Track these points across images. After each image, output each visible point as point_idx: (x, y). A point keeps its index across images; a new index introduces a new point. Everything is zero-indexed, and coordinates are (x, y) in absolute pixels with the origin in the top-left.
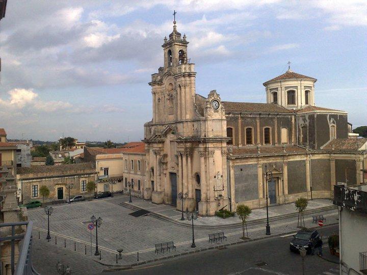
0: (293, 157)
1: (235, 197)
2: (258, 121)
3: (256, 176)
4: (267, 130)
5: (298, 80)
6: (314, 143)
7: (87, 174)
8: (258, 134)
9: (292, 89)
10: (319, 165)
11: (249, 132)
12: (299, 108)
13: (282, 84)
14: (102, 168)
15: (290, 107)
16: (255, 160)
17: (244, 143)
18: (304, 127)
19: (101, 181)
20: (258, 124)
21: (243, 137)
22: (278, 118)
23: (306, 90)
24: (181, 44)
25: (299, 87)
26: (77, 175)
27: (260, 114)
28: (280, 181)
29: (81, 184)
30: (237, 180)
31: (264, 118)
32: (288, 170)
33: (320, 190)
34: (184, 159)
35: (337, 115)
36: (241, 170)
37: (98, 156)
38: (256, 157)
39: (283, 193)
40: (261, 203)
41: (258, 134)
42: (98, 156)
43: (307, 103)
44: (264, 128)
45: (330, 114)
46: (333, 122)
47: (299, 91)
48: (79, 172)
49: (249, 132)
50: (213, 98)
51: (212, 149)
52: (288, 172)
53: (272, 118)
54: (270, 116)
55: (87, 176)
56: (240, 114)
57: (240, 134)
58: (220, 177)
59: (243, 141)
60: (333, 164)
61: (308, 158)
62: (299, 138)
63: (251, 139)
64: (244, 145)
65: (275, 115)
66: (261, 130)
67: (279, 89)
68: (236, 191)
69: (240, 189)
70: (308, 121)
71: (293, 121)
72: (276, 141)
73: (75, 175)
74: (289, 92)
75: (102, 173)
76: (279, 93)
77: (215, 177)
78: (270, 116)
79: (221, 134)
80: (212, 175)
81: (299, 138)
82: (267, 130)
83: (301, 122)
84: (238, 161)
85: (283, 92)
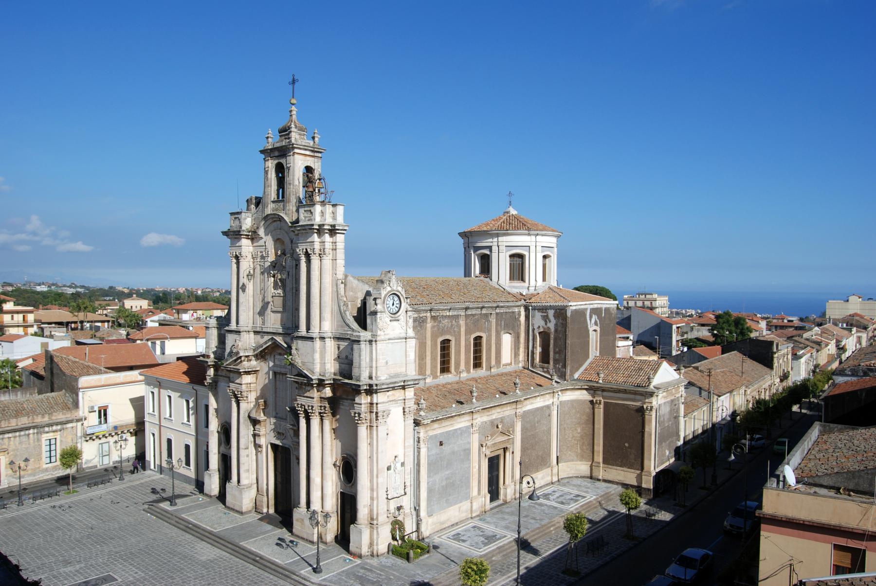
0: (531, 401)
1: (427, 504)
2: (462, 322)
3: (467, 452)
4: (478, 341)
5: (529, 235)
6: (564, 366)
7: (57, 424)
8: (461, 353)
10: (574, 411)
11: (445, 345)
12: (532, 289)
13: (500, 239)
14: (93, 407)
15: (514, 287)
16: (467, 418)
17: (436, 373)
19: (90, 437)
20: (463, 329)
21: (433, 359)
22: (497, 314)
23: (545, 253)
24: (308, 153)
25: (533, 249)
26: (34, 427)
27: (467, 309)
29: (45, 448)
30: (433, 466)
31: (473, 315)
32: (522, 430)
33: (573, 461)
34: (315, 422)
35: (601, 309)
36: (441, 444)
37: (83, 381)
38: (469, 412)
39: (513, 477)
40: (474, 508)
41: (461, 353)
42: (83, 381)
43: (544, 280)
44: (473, 336)
45: (592, 306)
46: (596, 324)
48: (39, 420)
49: (445, 345)
50: (389, 289)
52: (522, 434)
53: (486, 315)
54: (484, 311)
55: (59, 427)
56: (431, 310)
57: (428, 353)
58: (399, 465)
59: (433, 367)
61: (555, 400)
63: (448, 362)
64: (435, 377)
65: (492, 307)
66: (467, 340)
68: (430, 491)
69: (437, 487)
71: (523, 318)
72: (493, 363)
73: (28, 428)
75: (93, 419)
78: (484, 311)
79: (403, 370)
80: (383, 465)
82: (478, 341)
83: (538, 321)
84: (436, 425)
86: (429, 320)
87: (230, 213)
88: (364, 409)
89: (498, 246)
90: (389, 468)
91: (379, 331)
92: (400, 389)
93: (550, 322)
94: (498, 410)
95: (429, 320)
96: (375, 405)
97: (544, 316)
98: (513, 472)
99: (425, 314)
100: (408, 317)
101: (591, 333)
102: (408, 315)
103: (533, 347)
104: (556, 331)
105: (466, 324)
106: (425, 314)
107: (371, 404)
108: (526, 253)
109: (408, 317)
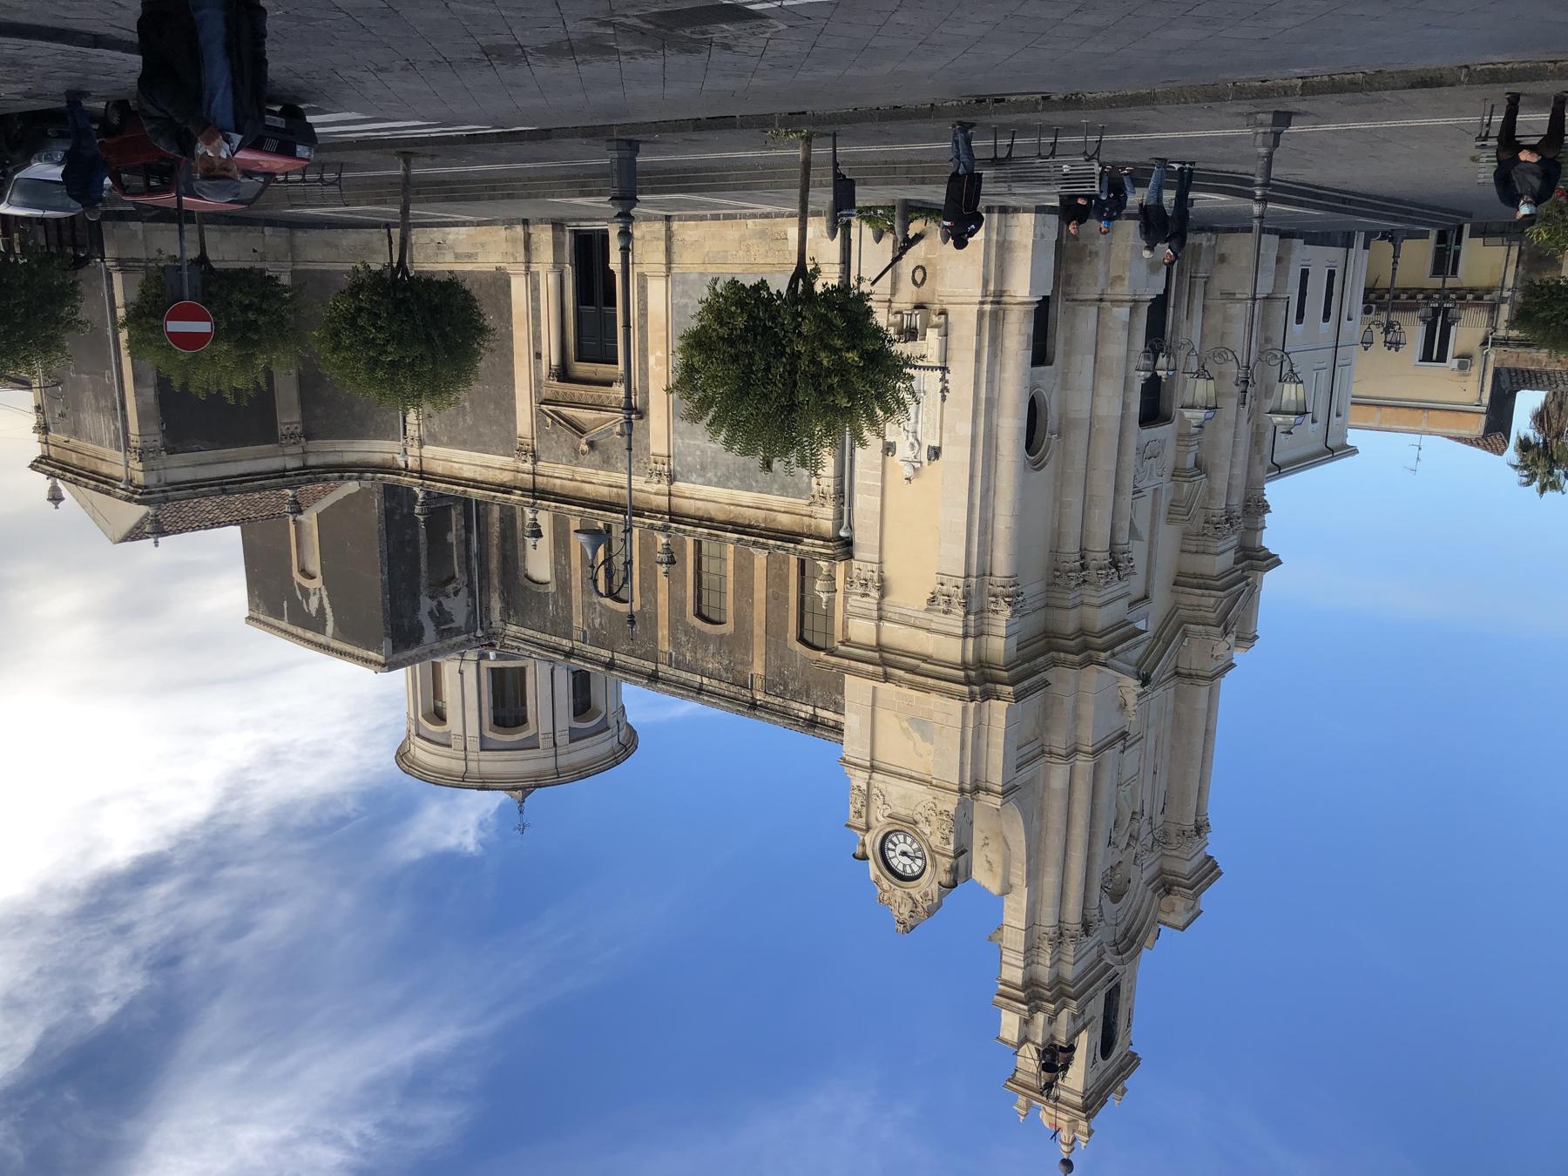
2: (664, 646)
9: (508, 738)
12: (472, 655)
13: (549, 764)
14: (1462, 367)
18: (441, 584)
22: (569, 636)
25: (474, 745)
28: (554, 362)
46: (306, 593)
47: (473, 730)
51: (938, 620)
60: (289, 418)
62: (468, 529)
67: (563, 739)
70: (424, 618)
74: (520, 721)
76: (565, 719)
77: (935, 453)
78: (605, 654)
81: (468, 529)
83: (458, 607)
84: (785, 521)
85: (545, 726)
86: (758, 683)
87: (1202, 911)
88: (1001, 620)
89: (555, 745)
90: (935, 453)
91: (952, 812)
92: (887, 648)
93: (431, 613)
94: (590, 490)
95: (758, 683)
96: (972, 631)
97: (446, 623)
98: (535, 298)
99: (768, 699)
100: (864, 814)
101: (314, 565)
102: (864, 820)
103: (468, 542)
104: (415, 596)
105: (655, 640)
106: (768, 699)
107: (980, 634)
108: (489, 734)
109: (864, 814)
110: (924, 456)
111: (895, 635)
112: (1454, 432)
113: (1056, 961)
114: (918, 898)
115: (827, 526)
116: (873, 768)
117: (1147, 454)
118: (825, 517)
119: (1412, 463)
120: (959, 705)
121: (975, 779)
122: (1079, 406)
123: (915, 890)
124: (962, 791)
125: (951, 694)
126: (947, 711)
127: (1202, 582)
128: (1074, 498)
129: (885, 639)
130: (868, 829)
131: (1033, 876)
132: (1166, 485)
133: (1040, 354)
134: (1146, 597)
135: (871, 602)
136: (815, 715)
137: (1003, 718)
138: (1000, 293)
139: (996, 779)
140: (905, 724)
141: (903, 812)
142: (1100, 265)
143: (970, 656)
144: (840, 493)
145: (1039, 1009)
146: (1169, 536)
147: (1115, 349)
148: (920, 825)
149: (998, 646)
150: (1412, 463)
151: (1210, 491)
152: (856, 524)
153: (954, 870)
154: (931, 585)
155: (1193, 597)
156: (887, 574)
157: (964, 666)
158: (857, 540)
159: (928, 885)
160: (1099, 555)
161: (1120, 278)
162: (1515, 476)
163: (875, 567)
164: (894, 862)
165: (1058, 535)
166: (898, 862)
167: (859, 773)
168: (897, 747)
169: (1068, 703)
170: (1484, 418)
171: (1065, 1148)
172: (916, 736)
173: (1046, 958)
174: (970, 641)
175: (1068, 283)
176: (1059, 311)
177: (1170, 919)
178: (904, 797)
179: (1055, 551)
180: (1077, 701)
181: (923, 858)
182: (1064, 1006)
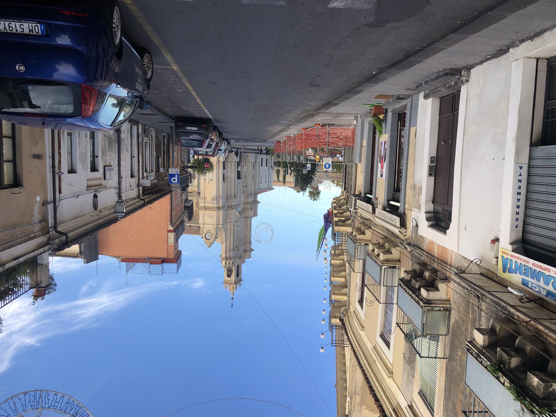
77: (212, 180)
88: (221, 201)
90: (212, 180)
110: (210, 180)
111: (207, 205)
112: (290, 186)
113: (230, 254)
114: (211, 242)
115: (197, 191)
116: (204, 224)
117: (238, 183)
118: (196, 189)
119: (285, 192)
120: (216, 212)
121: (218, 223)
122: (229, 175)
123: (210, 241)
124: (217, 225)
125: (215, 211)
126: (214, 213)
127: (248, 203)
128: (229, 187)
129: (205, 206)
130: (203, 233)
131: (226, 241)
132: (242, 188)
133: (224, 169)
134: (240, 205)
135: (203, 201)
136: (190, 225)
137: (222, 214)
138: (219, 160)
139: (221, 223)
140: (208, 217)
141: (208, 230)
142: (231, 157)
143: (217, 207)
144: (198, 186)
145: (227, 260)
146: (242, 196)
147: (233, 168)
148: (211, 231)
149: (221, 205)
150: (285, 192)
151: (248, 190)
152: (201, 190)
153: (216, 237)
154: (212, 197)
155: (247, 206)
156: (205, 196)
157: (217, 207)
158: (201, 192)
159: (212, 239)
160: (233, 195)
161: (233, 159)
162: (309, 198)
163: (204, 196)
164: (207, 238)
165: (227, 192)
166: (208, 237)
167: (202, 225)
168: (207, 220)
169: (230, 215)
170: (294, 183)
171: (232, 295)
172: (210, 218)
173: (228, 253)
174: (217, 204)
175: (227, 159)
176: (226, 163)
177: (247, 257)
178: (208, 228)
179: (227, 194)
180: (231, 215)
181: (211, 236)
182: (231, 260)
